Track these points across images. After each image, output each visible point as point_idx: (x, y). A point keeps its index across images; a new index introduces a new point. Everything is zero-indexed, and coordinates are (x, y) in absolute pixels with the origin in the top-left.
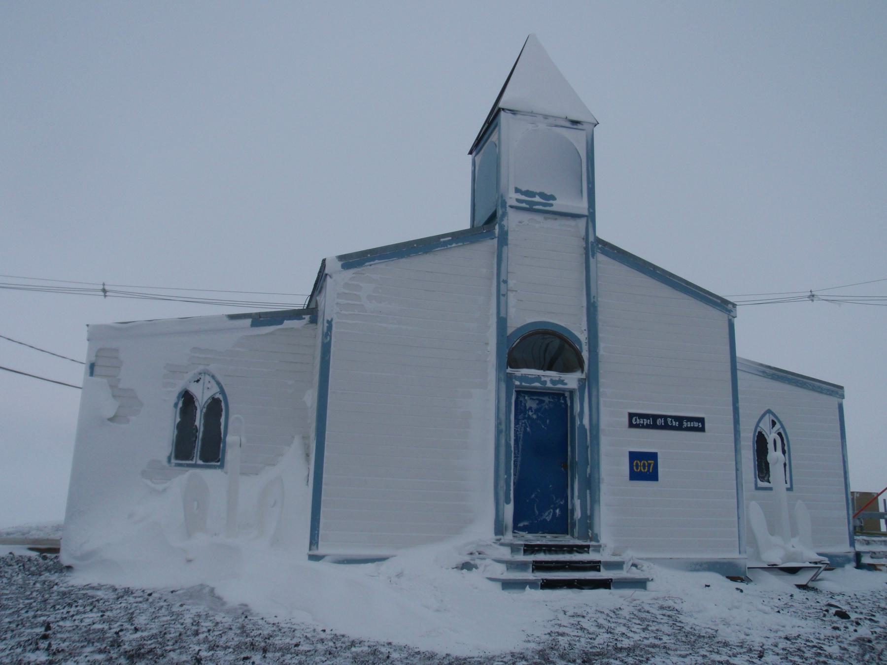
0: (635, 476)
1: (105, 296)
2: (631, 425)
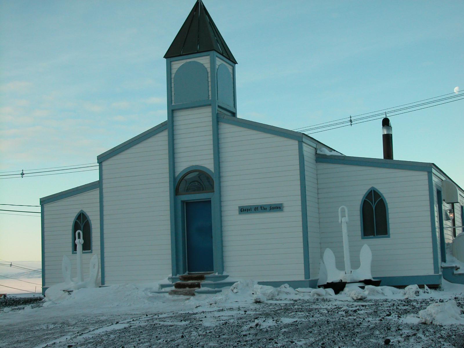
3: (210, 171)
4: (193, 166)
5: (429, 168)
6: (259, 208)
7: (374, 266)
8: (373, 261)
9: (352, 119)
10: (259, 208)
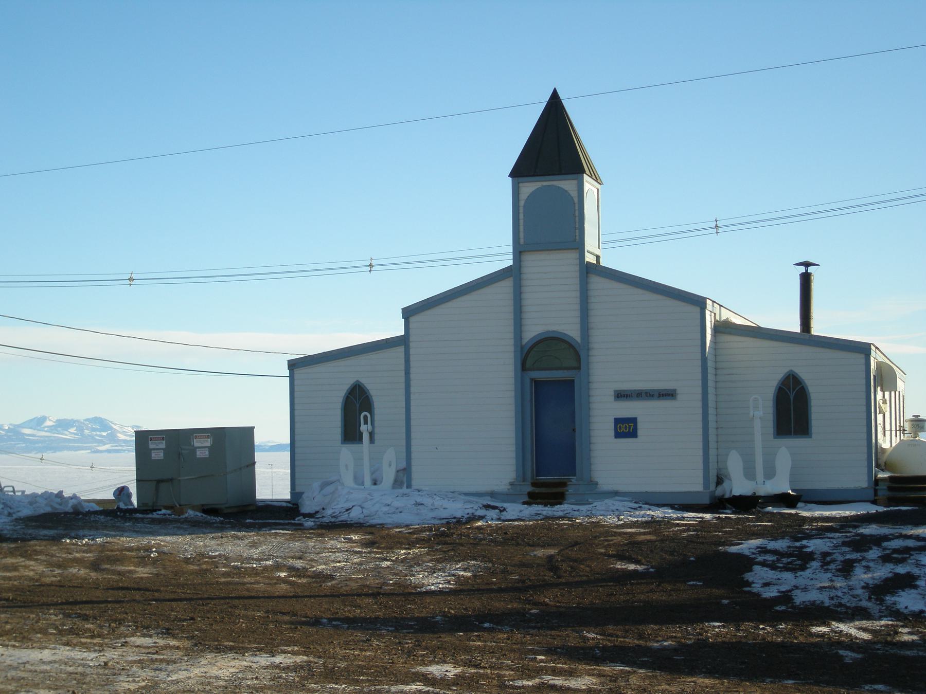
0: (618, 435)
4: (548, 332)
5: (864, 349)
6: (643, 395)
9: (719, 224)
10: (643, 395)
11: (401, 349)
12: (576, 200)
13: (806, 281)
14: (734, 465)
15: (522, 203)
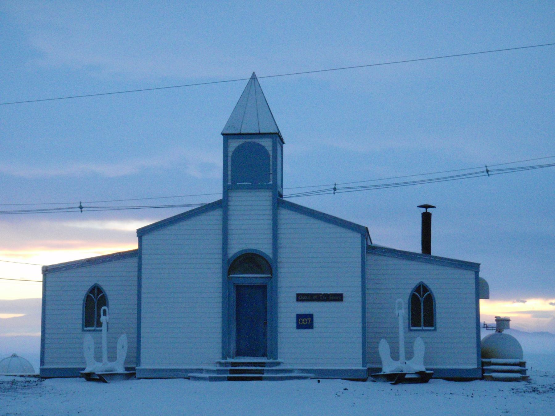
0: (299, 327)
1: (82, 211)
2: (298, 300)
3: (268, 256)
4: (249, 249)
7: (427, 359)
8: (426, 354)
11: (135, 260)
12: (271, 153)
13: (427, 219)
14: (384, 349)
15: (230, 154)
